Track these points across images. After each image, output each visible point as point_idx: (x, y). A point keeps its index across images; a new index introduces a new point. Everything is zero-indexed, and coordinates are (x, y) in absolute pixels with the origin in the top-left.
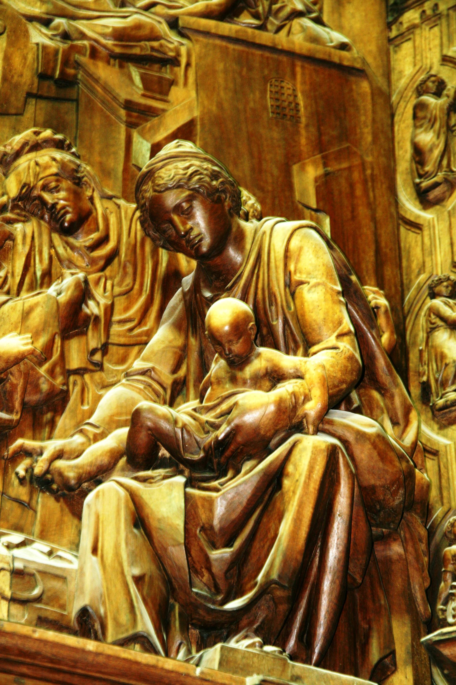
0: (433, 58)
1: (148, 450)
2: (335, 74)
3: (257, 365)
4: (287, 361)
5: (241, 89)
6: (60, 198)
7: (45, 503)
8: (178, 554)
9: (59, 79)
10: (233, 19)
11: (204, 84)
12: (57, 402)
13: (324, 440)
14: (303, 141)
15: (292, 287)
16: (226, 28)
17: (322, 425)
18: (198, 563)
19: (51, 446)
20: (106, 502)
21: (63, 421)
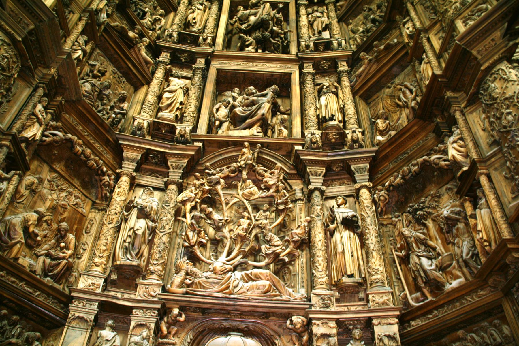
0: (93, 217)
1: (48, 255)
2: (83, 216)
3: (63, 251)
4: (66, 252)
5: (73, 214)
6: (49, 222)
7: (34, 256)
8: (47, 268)
9: (322, 145)
10: (187, 255)
11: (69, 213)
12: (40, 245)
13: (67, 261)
14: (77, 222)
15: (70, 243)
16: (74, 207)
17: (67, 260)
18: (48, 269)
19: (38, 250)
20: (41, 259)
21: (40, 247)
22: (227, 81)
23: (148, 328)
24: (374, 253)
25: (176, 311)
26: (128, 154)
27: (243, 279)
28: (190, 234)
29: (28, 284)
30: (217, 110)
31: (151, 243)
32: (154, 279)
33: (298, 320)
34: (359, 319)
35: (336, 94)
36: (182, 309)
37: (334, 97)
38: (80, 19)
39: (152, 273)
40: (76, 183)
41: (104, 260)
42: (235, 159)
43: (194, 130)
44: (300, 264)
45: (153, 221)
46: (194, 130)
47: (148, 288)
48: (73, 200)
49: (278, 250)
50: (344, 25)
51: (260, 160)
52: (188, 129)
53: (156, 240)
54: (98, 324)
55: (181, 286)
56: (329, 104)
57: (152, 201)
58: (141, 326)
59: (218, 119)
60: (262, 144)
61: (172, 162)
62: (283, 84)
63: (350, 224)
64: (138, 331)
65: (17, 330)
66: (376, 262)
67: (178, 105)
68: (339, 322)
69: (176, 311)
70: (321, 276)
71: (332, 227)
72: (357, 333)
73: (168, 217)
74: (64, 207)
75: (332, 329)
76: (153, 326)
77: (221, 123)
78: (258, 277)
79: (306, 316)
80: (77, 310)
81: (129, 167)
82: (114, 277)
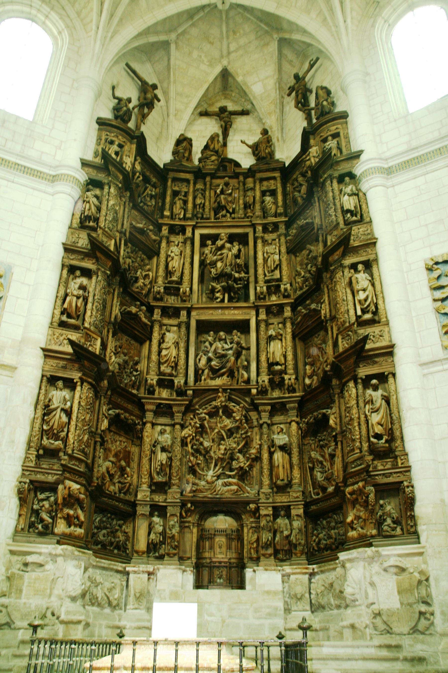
22: (204, 327)
23: (177, 516)
24: (295, 467)
25: (189, 505)
26: (147, 407)
27: (223, 485)
28: (192, 458)
29: (117, 501)
30: (200, 360)
31: (170, 466)
32: (174, 489)
33: (252, 506)
34: (284, 506)
35: (281, 340)
36: (191, 503)
37: (280, 342)
38: (108, 332)
39: (174, 485)
40: (122, 433)
41: (147, 480)
42: (214, 399)
43: (186, 383)
44: (255, 471)
45: (170, 452)
46: (186, 383)
47: (173, 496)
48: (123, 445)
49: (242, 465)
50: (293, 257)
51: (230, 399)
52: (182, 382)
53: (173, 464)
54: (151, 515)
55: (190, 493)
56: (276, 349)
57: (166, 439)
58: (172, 515)
59: (201, 369)
60: (231, 389)
61: (175, 409)
62: (243, 327)
63: (283, 448)
64: (171, 518)
65: (115, 522)
66: (296, 473)
67: (173, 359)
68: (274, 508)
69: (189, 505)
70: (266, 481)
71: (272, 450)
72: (282, 513)
73: (178, 448)
74: (120, 451)
75: (270, 511)
76: (178, 515)
77: (203, 371)
78: (230, 484)
79: (257, 504)
80: (140, 510)
81: (149, 416)
82: (153, 488)
